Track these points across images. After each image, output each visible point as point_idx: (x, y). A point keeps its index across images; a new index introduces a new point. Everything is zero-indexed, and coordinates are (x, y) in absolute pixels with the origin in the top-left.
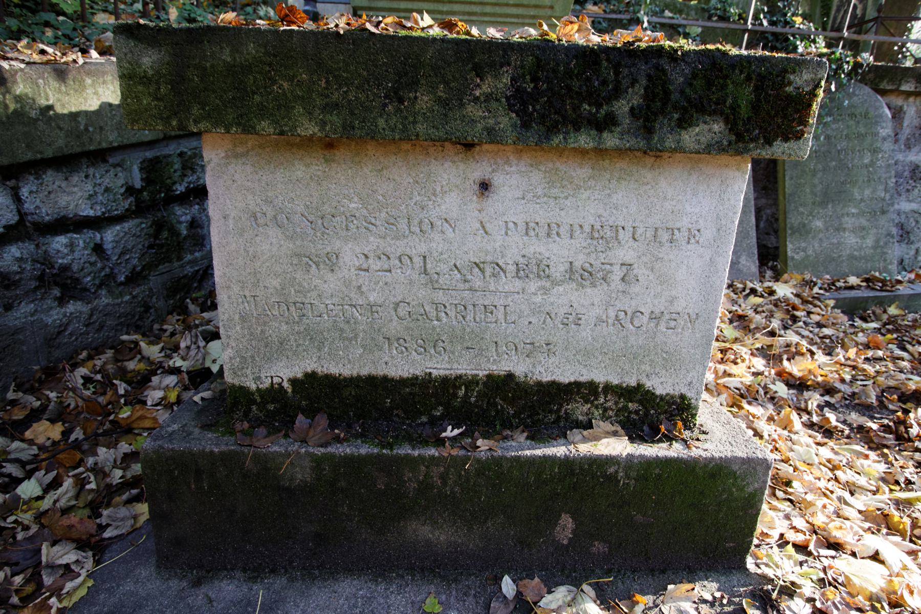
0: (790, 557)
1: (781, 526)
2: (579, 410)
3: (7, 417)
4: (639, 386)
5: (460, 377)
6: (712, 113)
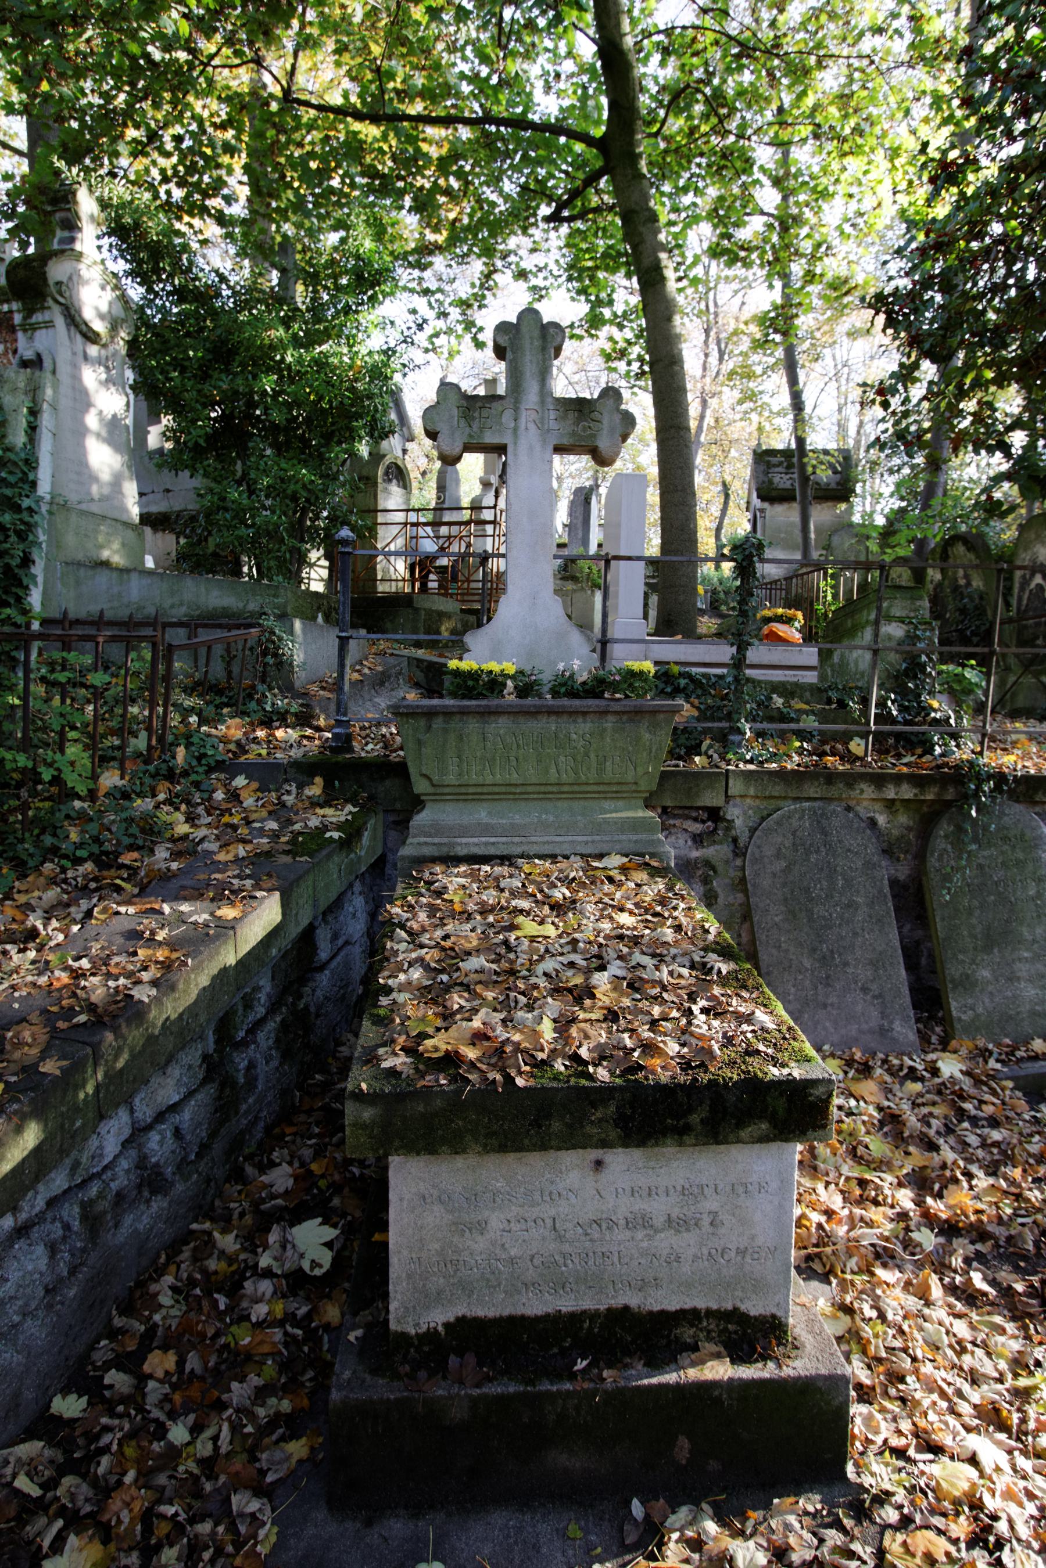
0: (887, 1465)
1: (885, 1431)
2: (687, 1334)
3: (120, 1349)
4: (736, 1309)
5: (584, 1312)
6: (760, 1118)
